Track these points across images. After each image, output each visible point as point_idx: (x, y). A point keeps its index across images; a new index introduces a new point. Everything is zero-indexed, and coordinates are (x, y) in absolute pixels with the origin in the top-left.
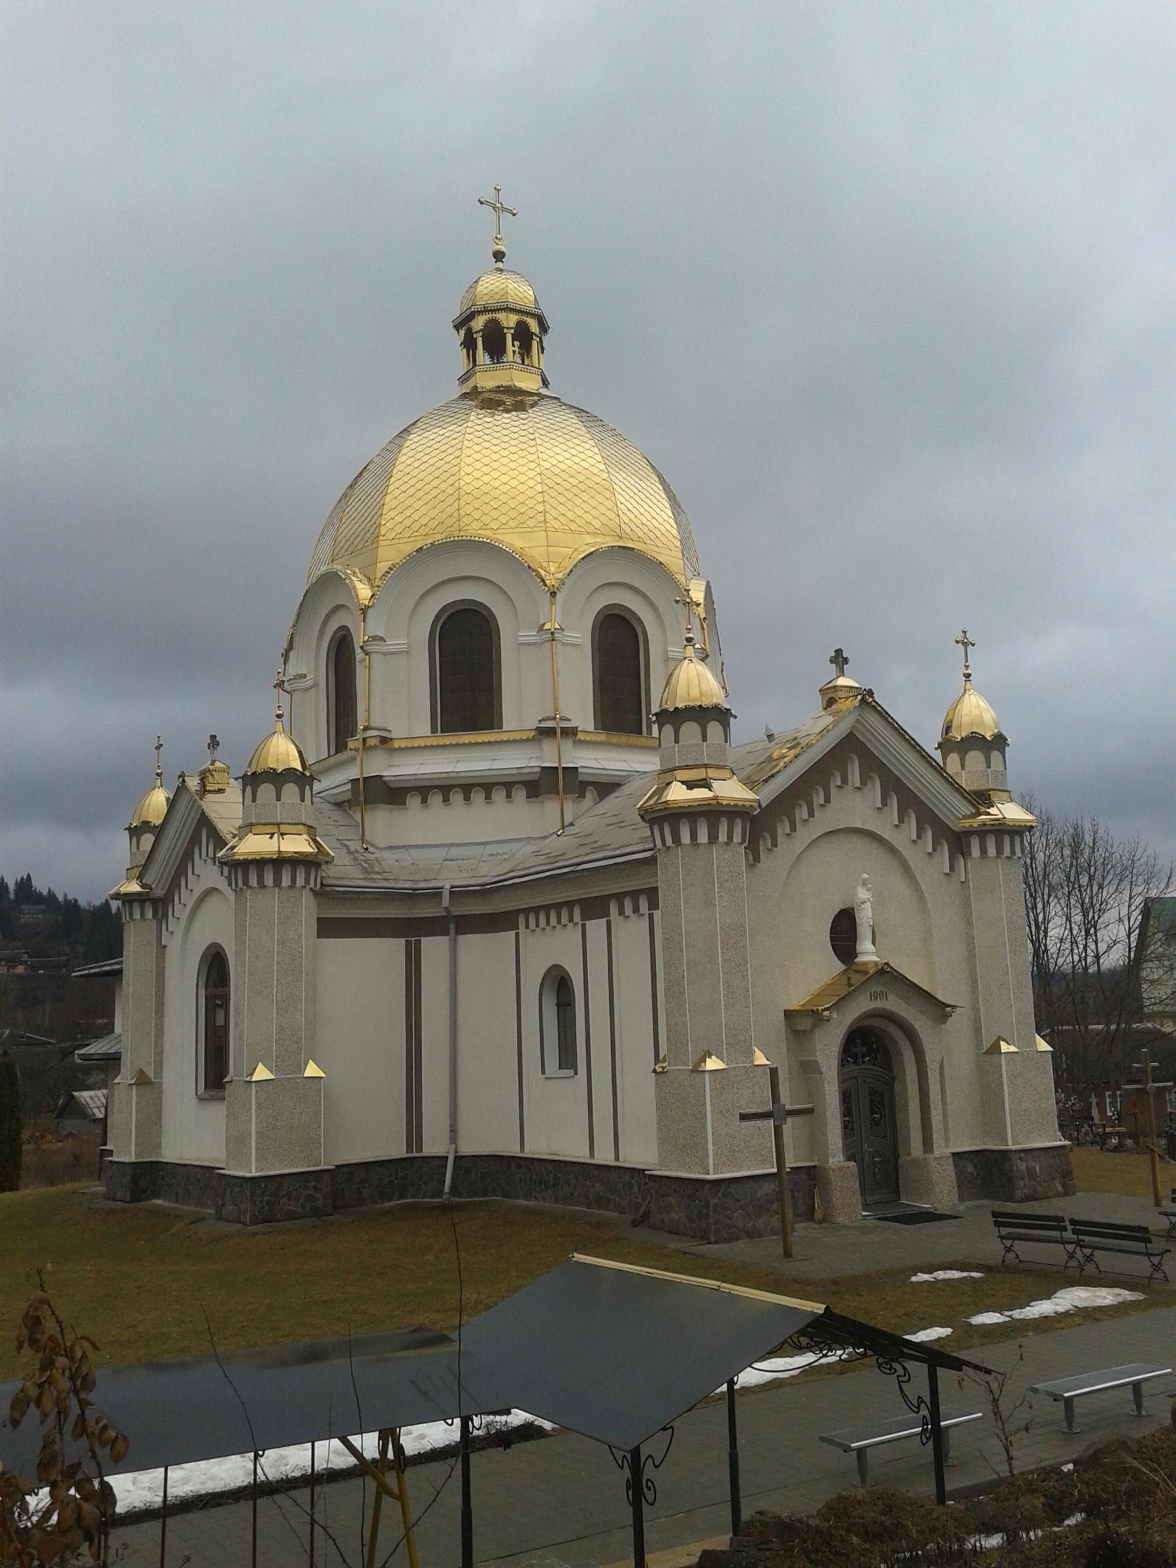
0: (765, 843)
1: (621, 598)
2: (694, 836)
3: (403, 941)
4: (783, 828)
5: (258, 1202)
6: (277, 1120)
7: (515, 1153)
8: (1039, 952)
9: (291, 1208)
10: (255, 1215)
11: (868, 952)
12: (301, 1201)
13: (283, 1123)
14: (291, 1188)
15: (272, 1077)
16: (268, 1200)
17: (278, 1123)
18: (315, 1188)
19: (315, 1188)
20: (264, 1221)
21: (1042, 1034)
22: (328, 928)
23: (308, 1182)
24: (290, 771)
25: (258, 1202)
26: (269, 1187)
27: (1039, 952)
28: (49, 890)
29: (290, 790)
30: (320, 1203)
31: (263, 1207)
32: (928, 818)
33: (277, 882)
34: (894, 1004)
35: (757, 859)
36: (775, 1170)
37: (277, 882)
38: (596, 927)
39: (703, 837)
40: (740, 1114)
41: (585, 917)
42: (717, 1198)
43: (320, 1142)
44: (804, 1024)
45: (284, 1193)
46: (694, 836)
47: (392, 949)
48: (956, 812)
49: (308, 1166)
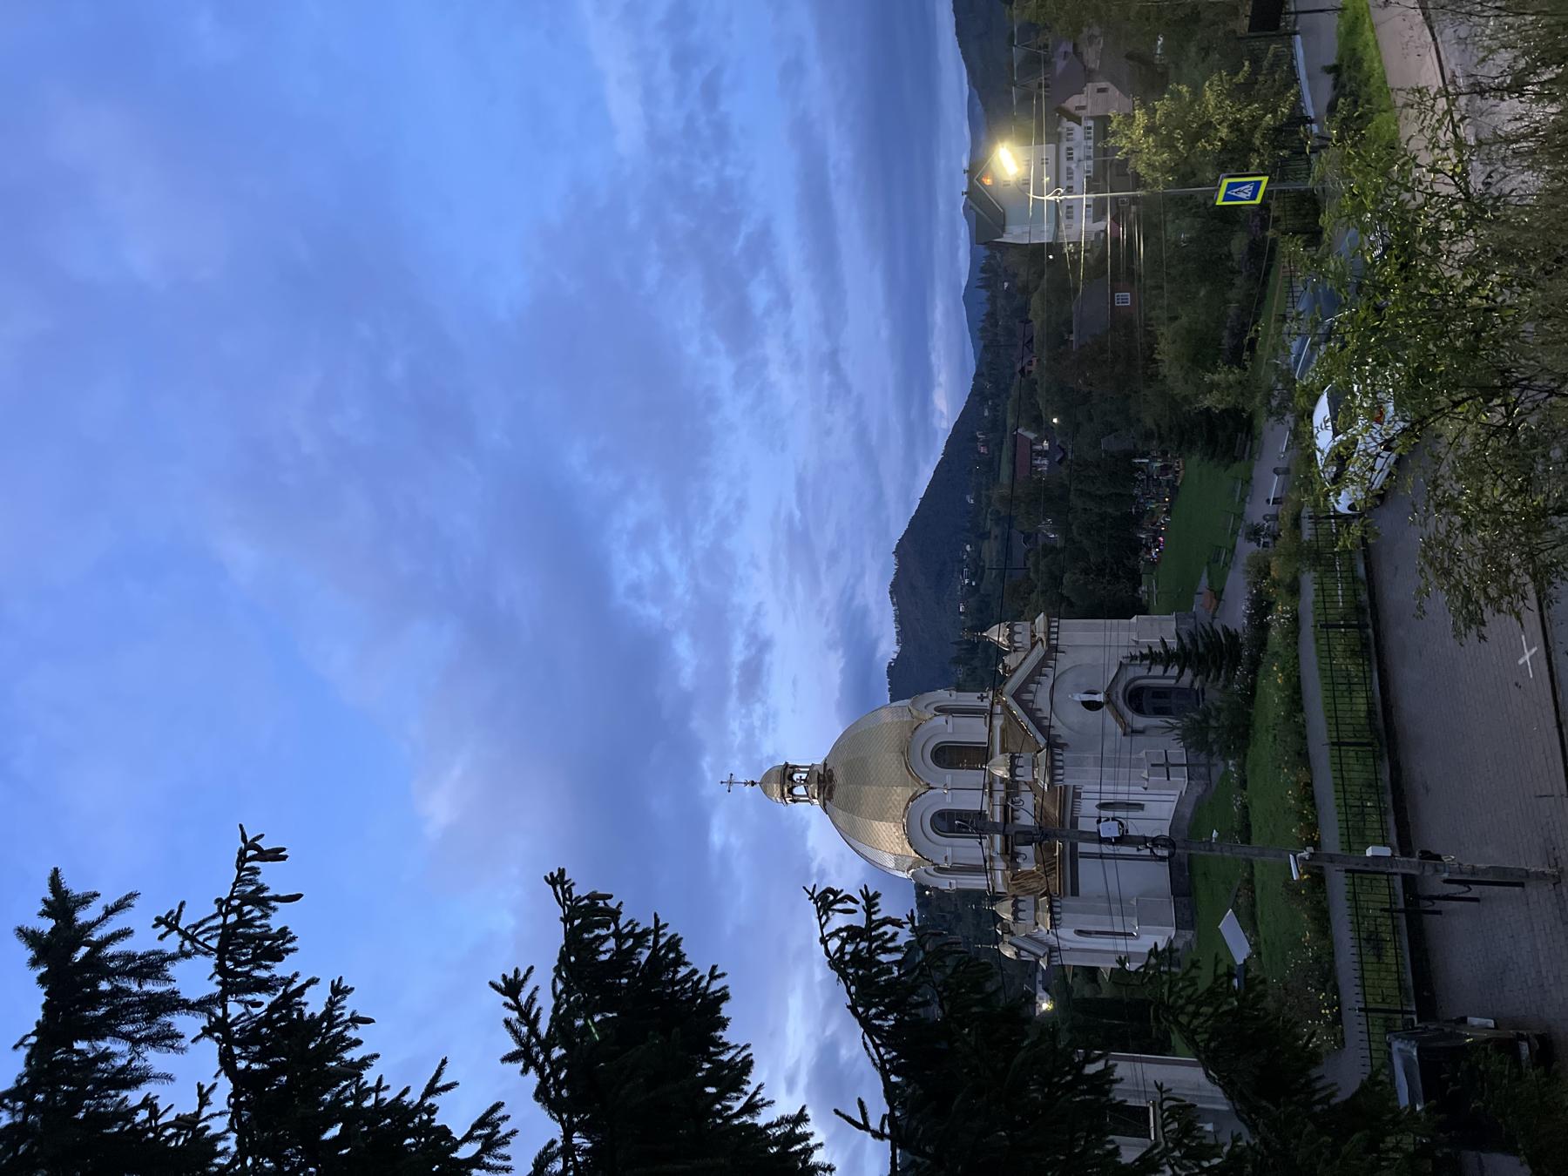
0: (1060, 741)
1: (930, 761)
3: (1080, 860)
4: (1052, 732)
7: (1171, 810)
11: (1100, 698)
22: (1075, 892)
24: (1013, 905)
28: (728, 1019)
29: (1020, 906)
32: (1042, 663)
33: (1059, 913)
34: (1120, 689)
35: (1066, 745)
36: (1186, 768)
37: (1059, 913)
38: (1083, 796)
39: (1061, 771)
41: (1080, 798)
44: (1129, 730)
47: (1083, 863)
48: (1040, 650)
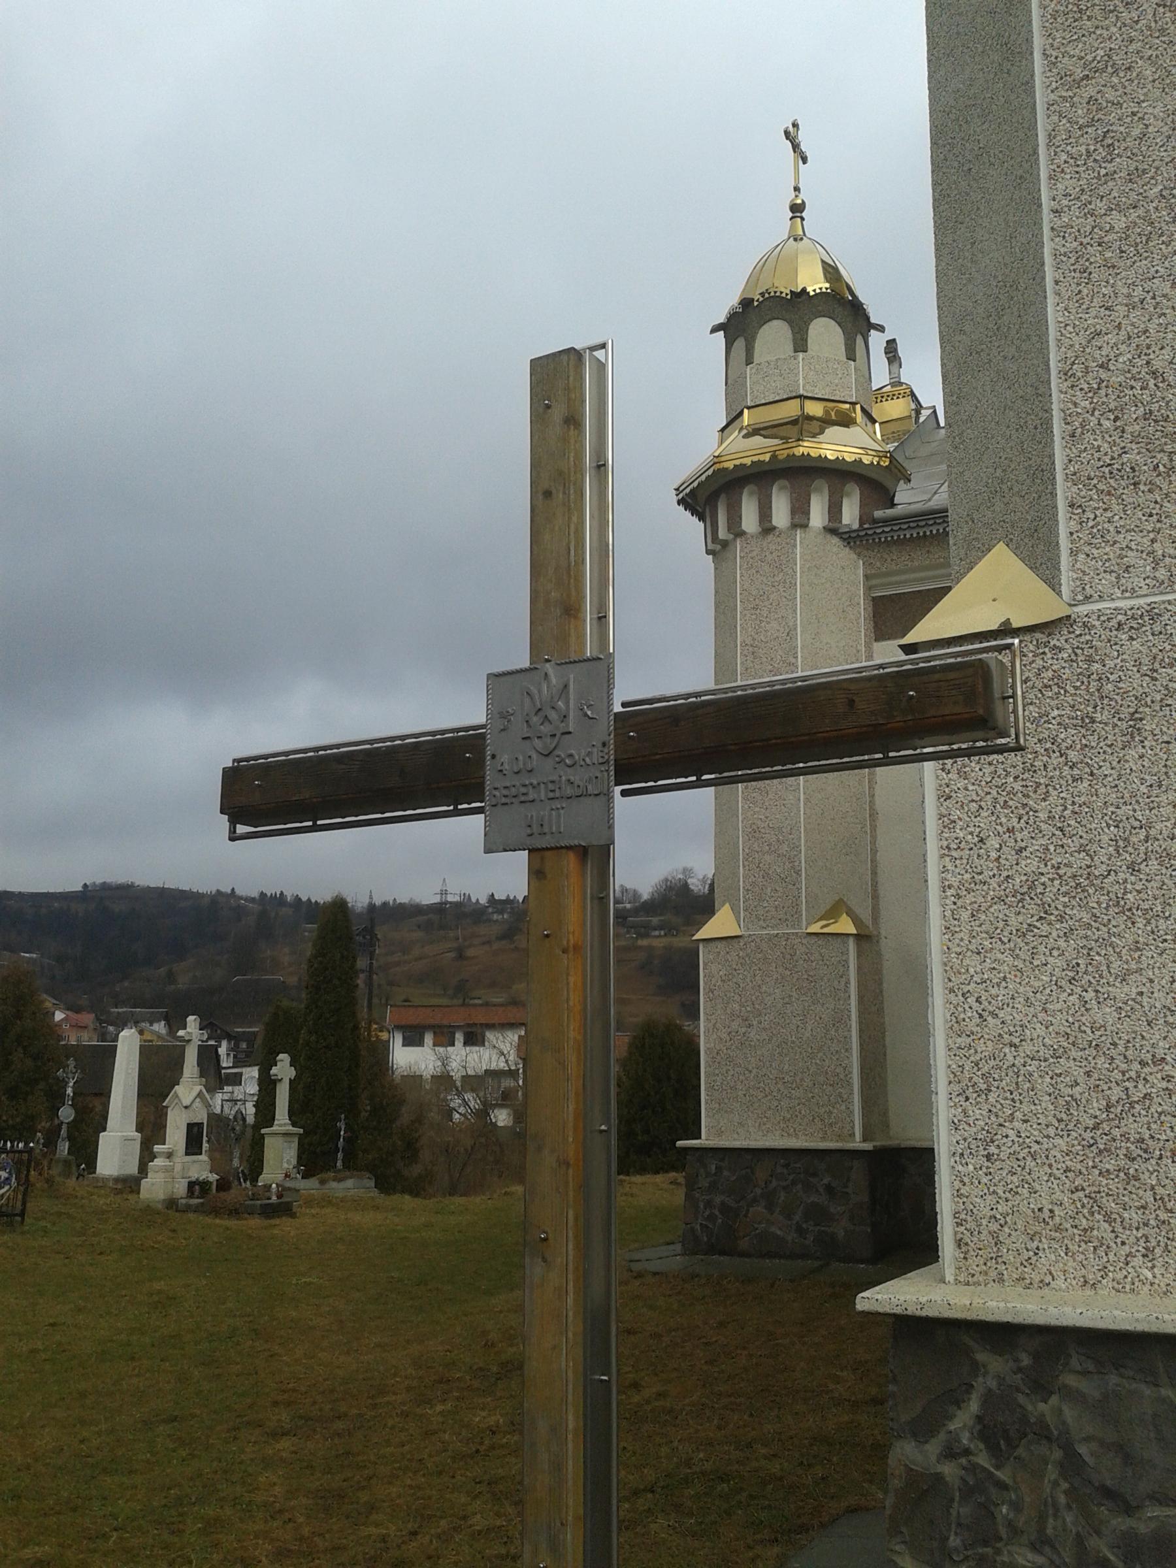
2: (765, 514)
5: (702, 1205)
6: (750, 1026)
8: (458, 1006)
9: (773, 1229)
10: (693, 1230)
12: (797, 1218)
13: (764, 1036)
14: (774, 1183)
15: (736, 932)
16: (723, 1203)
17: (752, 1034)
18: (829, 1189)
19: (829, 1189)
20: (712, 1249)
21: (197, 1187)
23: (815, 1175)
25: (702, 1205)
26: (726, 1173)
27: (458, 1006)
30: (840, 1229)
31: (713, 1218)
39: (781, 515)
40: (293, 1215)
42: (933, 1448)
43: (850, 1084)
45: (758, 1191)
46: (765, 514)
49: (823, 1139)
